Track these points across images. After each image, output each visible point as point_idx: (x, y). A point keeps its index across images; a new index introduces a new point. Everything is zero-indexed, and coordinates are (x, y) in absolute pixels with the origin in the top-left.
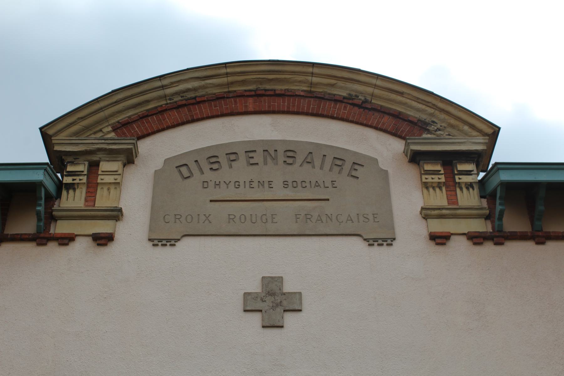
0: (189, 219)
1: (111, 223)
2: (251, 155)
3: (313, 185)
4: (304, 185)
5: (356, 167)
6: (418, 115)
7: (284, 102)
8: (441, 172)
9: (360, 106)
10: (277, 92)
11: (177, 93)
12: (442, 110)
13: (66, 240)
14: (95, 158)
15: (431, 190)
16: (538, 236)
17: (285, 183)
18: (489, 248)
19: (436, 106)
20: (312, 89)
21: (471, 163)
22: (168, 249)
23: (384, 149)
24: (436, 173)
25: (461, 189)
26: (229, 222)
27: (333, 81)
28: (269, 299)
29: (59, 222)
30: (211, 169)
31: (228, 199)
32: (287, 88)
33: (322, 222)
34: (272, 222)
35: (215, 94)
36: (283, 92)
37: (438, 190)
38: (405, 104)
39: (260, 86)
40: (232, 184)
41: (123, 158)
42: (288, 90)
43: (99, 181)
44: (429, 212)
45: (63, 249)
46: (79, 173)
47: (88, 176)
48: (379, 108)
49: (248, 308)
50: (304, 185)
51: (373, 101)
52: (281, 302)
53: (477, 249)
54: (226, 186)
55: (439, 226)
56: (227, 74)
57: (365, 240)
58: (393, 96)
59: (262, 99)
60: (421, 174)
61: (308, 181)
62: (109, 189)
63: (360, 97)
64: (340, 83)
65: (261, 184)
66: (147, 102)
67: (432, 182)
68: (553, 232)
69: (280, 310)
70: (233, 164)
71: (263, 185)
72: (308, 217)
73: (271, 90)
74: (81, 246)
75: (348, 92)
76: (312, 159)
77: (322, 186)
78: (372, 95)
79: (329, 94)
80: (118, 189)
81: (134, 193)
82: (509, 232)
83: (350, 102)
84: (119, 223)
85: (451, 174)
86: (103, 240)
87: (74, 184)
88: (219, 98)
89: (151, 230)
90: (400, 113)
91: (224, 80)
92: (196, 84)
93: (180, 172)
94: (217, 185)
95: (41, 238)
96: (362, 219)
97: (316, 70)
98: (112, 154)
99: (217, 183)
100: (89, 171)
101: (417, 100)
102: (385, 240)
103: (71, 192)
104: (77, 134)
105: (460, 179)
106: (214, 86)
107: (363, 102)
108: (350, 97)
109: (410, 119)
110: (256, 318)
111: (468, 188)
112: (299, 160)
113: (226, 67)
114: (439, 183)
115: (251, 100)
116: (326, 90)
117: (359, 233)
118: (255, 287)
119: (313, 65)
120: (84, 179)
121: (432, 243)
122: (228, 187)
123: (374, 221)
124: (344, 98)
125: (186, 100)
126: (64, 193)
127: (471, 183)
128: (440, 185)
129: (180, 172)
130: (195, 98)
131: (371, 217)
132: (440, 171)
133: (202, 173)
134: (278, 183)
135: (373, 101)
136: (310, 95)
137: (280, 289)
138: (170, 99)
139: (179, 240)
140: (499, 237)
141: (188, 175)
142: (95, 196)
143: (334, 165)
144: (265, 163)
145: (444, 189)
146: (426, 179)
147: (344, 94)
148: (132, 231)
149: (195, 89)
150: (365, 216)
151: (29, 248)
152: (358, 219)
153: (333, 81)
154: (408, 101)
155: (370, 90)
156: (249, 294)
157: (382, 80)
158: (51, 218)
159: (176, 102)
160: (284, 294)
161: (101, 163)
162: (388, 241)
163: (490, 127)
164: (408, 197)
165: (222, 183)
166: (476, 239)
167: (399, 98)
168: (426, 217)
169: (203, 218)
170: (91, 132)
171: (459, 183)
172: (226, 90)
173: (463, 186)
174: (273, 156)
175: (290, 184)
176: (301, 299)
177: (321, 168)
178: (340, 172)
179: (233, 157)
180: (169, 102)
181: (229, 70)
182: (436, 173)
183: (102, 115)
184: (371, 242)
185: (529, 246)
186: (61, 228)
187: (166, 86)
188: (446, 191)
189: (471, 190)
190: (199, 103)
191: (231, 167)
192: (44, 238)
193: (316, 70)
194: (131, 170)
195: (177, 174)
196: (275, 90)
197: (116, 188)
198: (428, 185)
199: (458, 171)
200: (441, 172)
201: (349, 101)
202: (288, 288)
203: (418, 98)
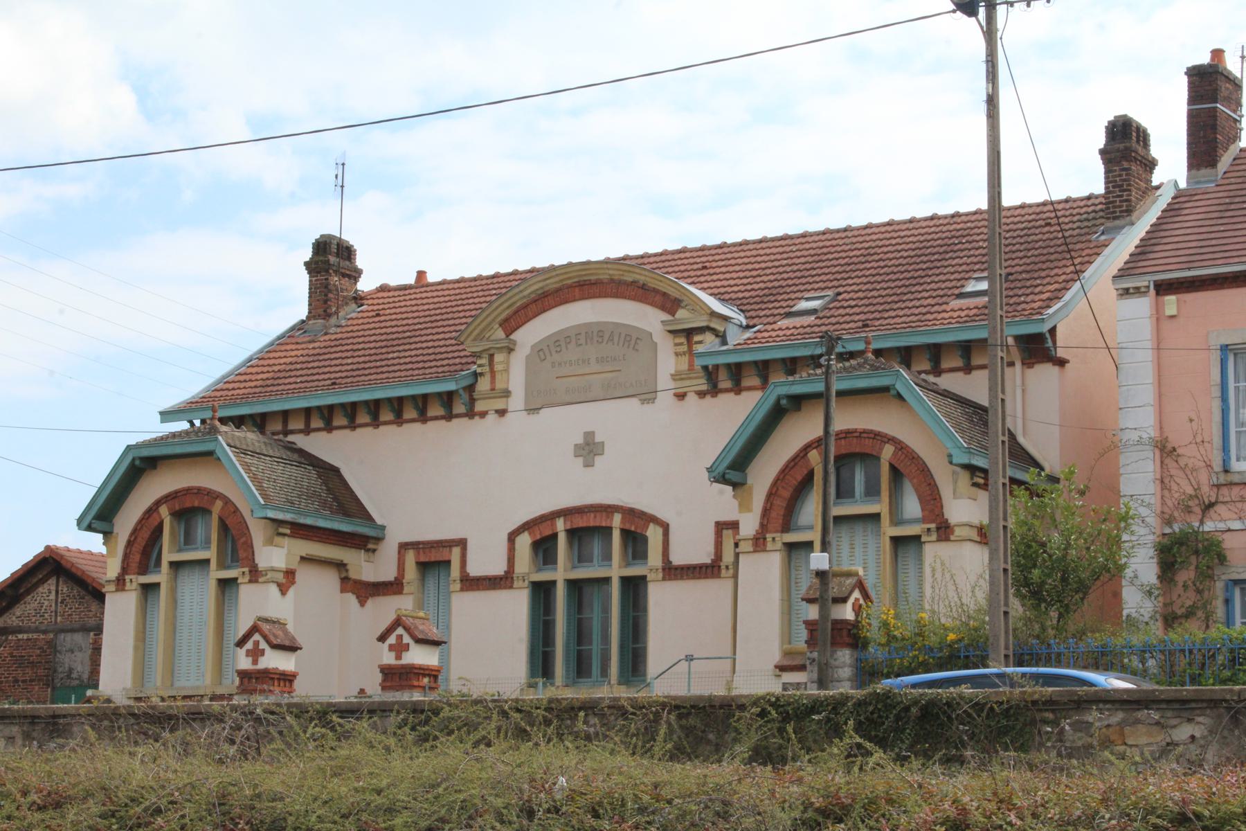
13: (483, 415)
18: (708, 397)
23: (649, 319)
24: (681, 344)
65: (584, 361)
74: (491, 417)
81: (516, 375)
86: (502, 413)
88: (558, 290)
91: (557, 279)
92: (541, 285)
94: (560, 364)
95: (471, 414)
104: (475, 340)
108: (634, 282)
110: (580, 460)
118: (580, 440)
128: (684, 353)
140: (714, 390)
147: (631, 280)
148: (517, 401)
158: (472, 401)
166: (702, 394)
182: (681, 344)
183: (489, 319)
194: (513, 355)
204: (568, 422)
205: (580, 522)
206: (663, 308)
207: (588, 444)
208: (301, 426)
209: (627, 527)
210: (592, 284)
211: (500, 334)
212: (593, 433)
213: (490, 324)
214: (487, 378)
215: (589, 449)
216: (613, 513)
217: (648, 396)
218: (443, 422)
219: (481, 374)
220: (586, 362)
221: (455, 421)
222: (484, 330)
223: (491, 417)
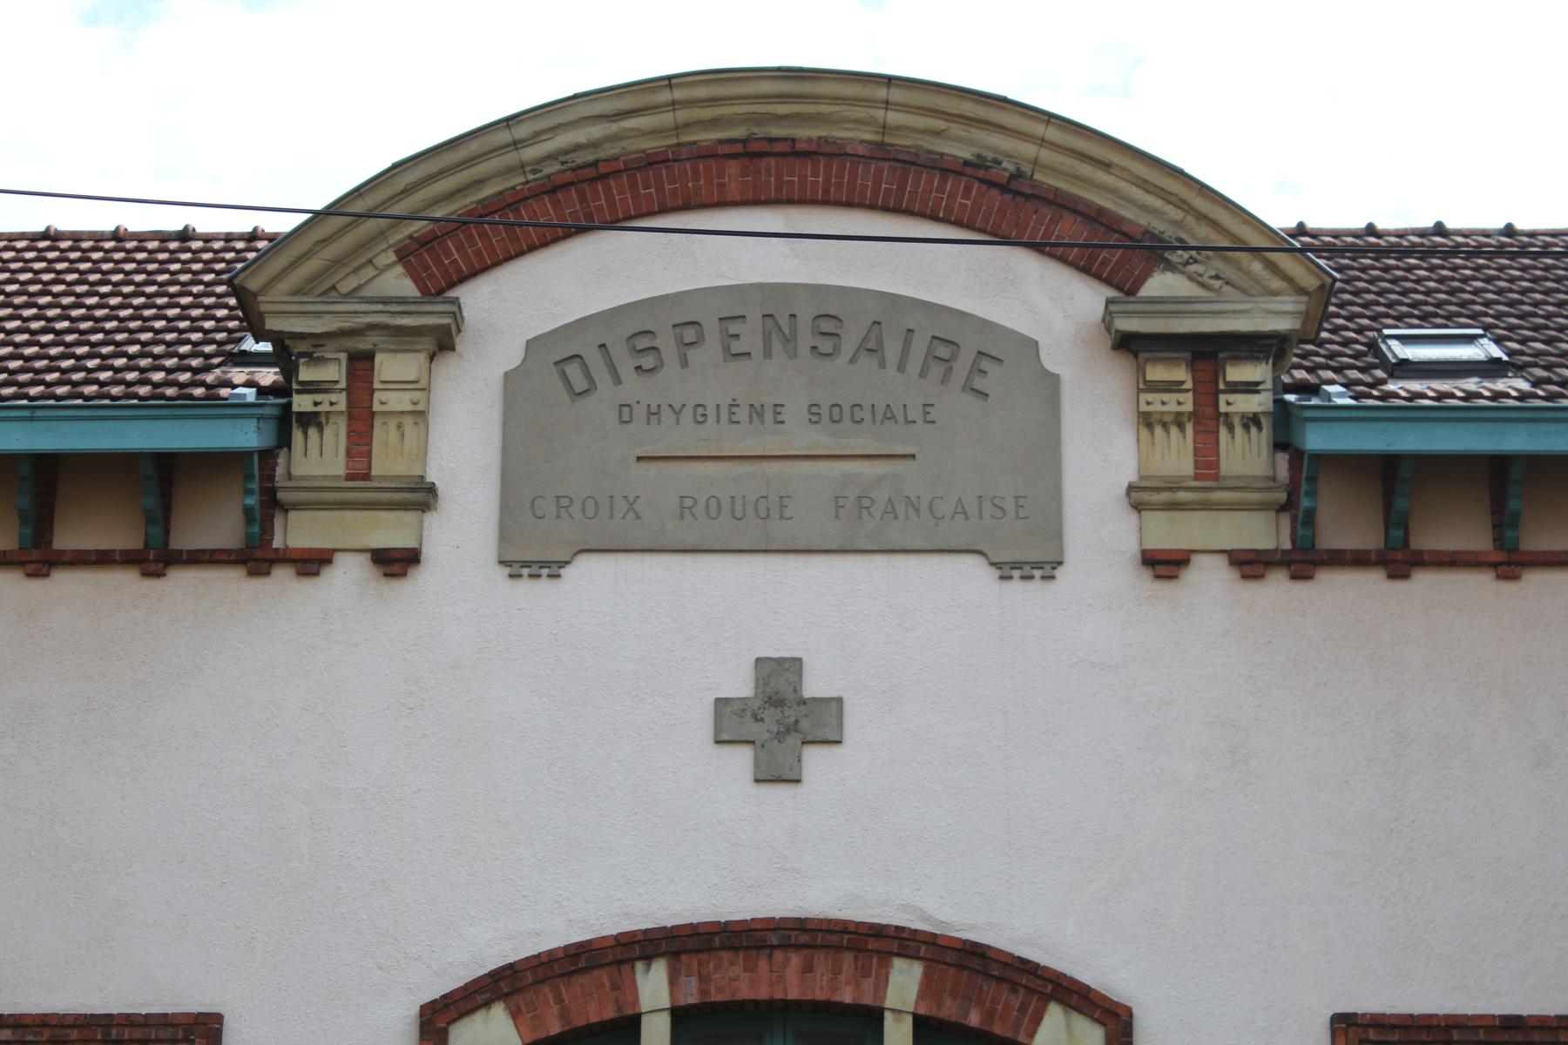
0: (590, 505)
1: (410, 517)
2: (734, 328)
3: (879, 417)
4: (858, 414)
5: (986, 364)
6: (1144, 220)
7: (815, 174)
8: (1184, 387)
9: (1004, 188)
10: (800, 147)
11: (551, 157)
12: (1202, 217)
13: (312, 563)
14: (363, 344)
15: (1159, 430)
16: (1394, 561)
17: (814, 410)
18: (1277, 588)
19: (1189, 205)
20: (888, 140)
21: (1258, 359)
22: (544, 585)
23: (1043, 303)
24: (1173, 387)
25: (1231, 428)
26: (682, 517)
27: (939, 124)
28: (771, 714)
29: (293, 516)
30: (639, 368)
31: (680, 453)
32: (823, 133)
33: (896, 517)
34: (781, 517)
35: (644, 151)
36: (814, 148)
37: (1174, 430)
38: (1114, 191)
39: (756, 130)
40: (688, 412)
41: (428, 343)
42: (826, 139)
43: (376, 407)
44: (1145, 496)
45: (308, 584)
46: (327, 386)
47: (349, 390)
48: (1051, 197)
49: (724, 737)
50: (858, 414)
51: (1036, 177)
52: (796, 722)
53: (1252, 588)
54: (673, 417)
55: (1167, 533)
56: (674, 105)
57: (992, 564)
58: (1086, 170)
59: (762, 163)
60: (1139, 391)
61: (866, 404)
62: (399, 426)
63: (1005, 165)
64: (957, 130)
65: (757, 412)
66: (479, 183)
67: (1162, 413)
68: (1429, 552)
69: (793, 740)
70: (692, 354)
71: (761, 416)
72: (863, 504)
73: (784, 139)
74: (349, 573)
75: (976, 150)
76: (880, 341)
77: (900, 418)
78: (1035, 162)
79: (929, 152)
80: (422, 426)
81: (460, 432)
82: (1327, 551)
83: (981, 173)
84: (431, 519)
85: (1208, 390)
86: (396, 563)
87: (317, 413)
88: (652, 161)
89: (504, 536)
90: (1101, 211)
91: (667, 118)
92: (597, 131)
93: (564, 375)
94: (653, 414)
95: (256, 557)
96: (988, 509)
97: (896, 95)
98: (403, 337)
99: (654, 409)
100: (351, 375)
101: (1143, 184)
102: (1038, 565)
103: (313, 432)
105: (1228, 404)
106: (643, 134)
107: (1012, 177)
108: (979, 164)
109: (1124, 228)
110: (742, 758)
111: (1246, 427)
112: (849, 345)
113: (670, 86)
114: (1178, 414)
115: (733, 168)
116: (920, 143)
117: (979, 548)
118: (741, 686)
119: (890, 81)
120: (341, 401)
121: (1147, 574)
122: (678, 422)
123: (1017, 517)
124: (967, 163)
125: (573, 170)
126: (297, 435)
127: (1255, 414)
128: (1179, 420)
129: (564, 375)
130: (595, 164)
131: (1009, 506)
132: (1183, 383)
133: (617, 380)
134: (795, 412)
135: (1036, 177)
136: (881, 152)
137: (795, 691)
138: (534, 171)
139: (568, 563)
140: (1304, 560)
141: (586, 387)
142: (369, 443)
143: (931, 356)
144: (768, 353)
145: (1189, 428)
146: (1148, 403)
147: (966, 153)
148: (462, 531)
149: (594, 145)
150: (997, 501)
151: (230, 580)
152: (980, 509)
153: (939, 124)
154: (1123, 185)
155: (1029, 150)
156: (727, 701)
157: (1061, 128)
158: (272, 504)
159: (548, 176)
160: (804, 702)
161: (378, 358)
162: (1046, 567)
163: (1312, 273)
164: (1102, 446)
165: (665, 408)
166: (1250, 565)
167: (1101, 176)
168: (1138, 507)
169: (621, 505)
170: (349, 269)
171: (1226, 414)
172: (674, 141)
173: (1236, 421)
174: (787, 331)
175: (825, 412)
176: (840, 715)
177: (901, 368)
178: (944, 381)
179: (689, 335)
180: (531, 177)
181: (678, 94)
182: (1173, 387)
184: (1007, 570)
185: (1372, 582)
186: (298, 532)
187: (523, 141)
188: (1196, 432)
189: (1254, 430)
190: (605, 177)
191: (685, 363)
192: (265, 560)
193: (896, 95)
194: (447, 367)
195: (558, 383)
196: (793, 140)
197: (416, 423)
198: (1154, 418)
199: (1226, 383)
200: (1184, 387)
201: (977, 171)
202: (814, 687)
203: (1146, 181)
204: (718, 613)
205: (742, 982)
206: (1087, 265)
207: (775, 701)
208: (123, 537)
209: (948, 1010)
210: (795, 152)
211: (398, 283)
212: (793, 666)
213: (363, 246)
214: (335, 436)
215: (779, 721)
216: (886, 957)
217: (1032, 559)
218: (125, 580)
219: (310, 420)
220: (766, 414)
221: (181, 580)
222: (338, 262)
223: (349, 573)
